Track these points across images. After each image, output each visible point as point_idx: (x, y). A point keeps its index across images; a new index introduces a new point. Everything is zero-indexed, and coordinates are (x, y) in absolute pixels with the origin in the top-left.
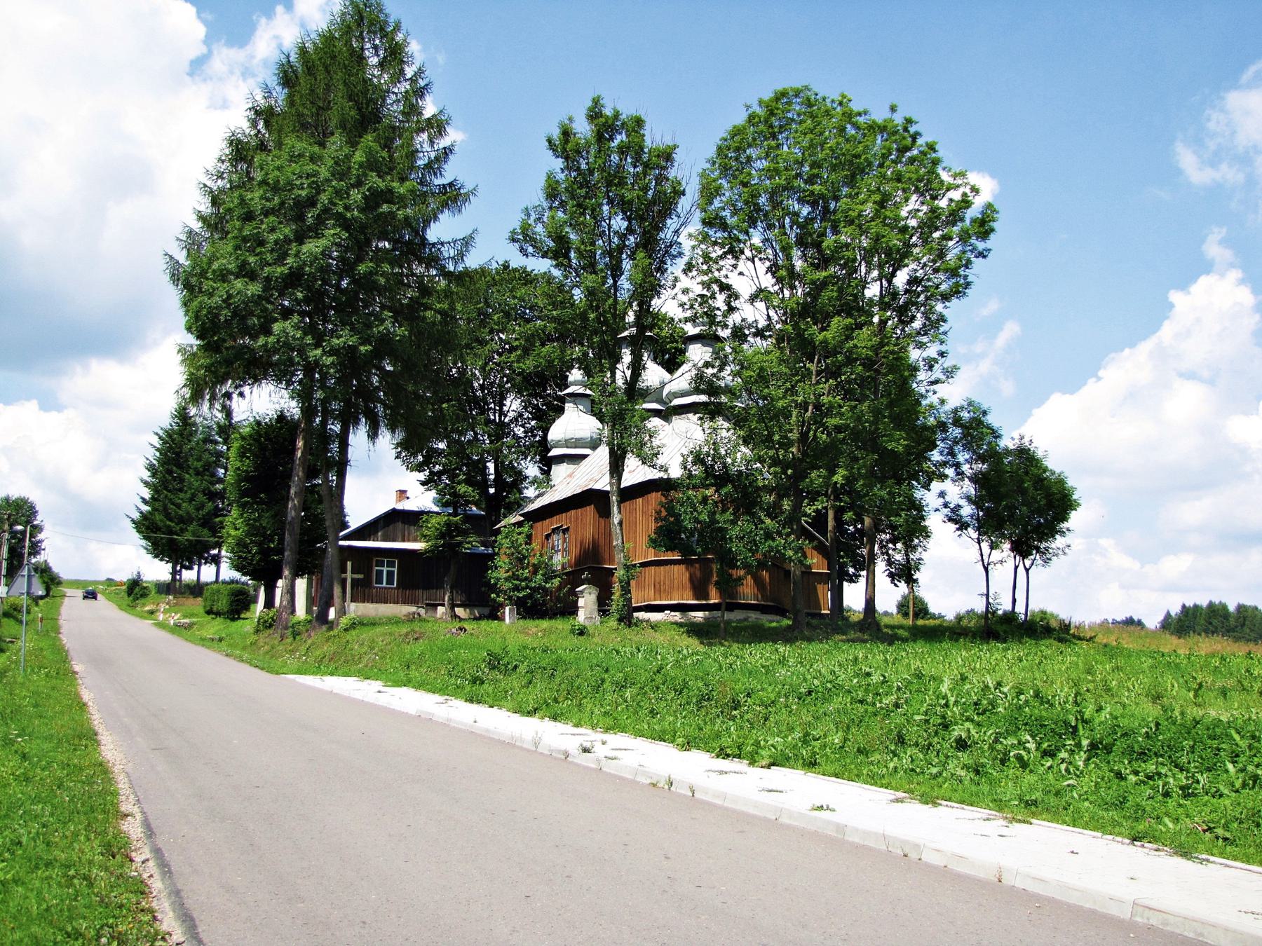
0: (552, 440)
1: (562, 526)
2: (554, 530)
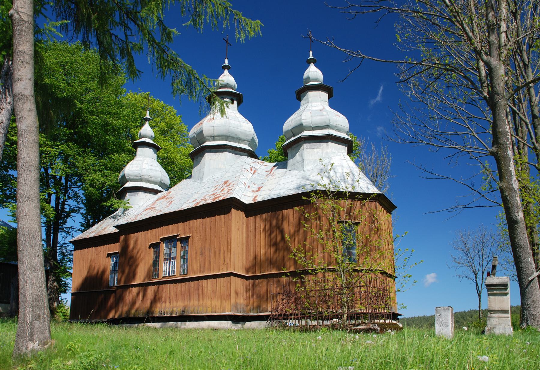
0: (129, 175)
1: (178, 235)
2: (163, 240)
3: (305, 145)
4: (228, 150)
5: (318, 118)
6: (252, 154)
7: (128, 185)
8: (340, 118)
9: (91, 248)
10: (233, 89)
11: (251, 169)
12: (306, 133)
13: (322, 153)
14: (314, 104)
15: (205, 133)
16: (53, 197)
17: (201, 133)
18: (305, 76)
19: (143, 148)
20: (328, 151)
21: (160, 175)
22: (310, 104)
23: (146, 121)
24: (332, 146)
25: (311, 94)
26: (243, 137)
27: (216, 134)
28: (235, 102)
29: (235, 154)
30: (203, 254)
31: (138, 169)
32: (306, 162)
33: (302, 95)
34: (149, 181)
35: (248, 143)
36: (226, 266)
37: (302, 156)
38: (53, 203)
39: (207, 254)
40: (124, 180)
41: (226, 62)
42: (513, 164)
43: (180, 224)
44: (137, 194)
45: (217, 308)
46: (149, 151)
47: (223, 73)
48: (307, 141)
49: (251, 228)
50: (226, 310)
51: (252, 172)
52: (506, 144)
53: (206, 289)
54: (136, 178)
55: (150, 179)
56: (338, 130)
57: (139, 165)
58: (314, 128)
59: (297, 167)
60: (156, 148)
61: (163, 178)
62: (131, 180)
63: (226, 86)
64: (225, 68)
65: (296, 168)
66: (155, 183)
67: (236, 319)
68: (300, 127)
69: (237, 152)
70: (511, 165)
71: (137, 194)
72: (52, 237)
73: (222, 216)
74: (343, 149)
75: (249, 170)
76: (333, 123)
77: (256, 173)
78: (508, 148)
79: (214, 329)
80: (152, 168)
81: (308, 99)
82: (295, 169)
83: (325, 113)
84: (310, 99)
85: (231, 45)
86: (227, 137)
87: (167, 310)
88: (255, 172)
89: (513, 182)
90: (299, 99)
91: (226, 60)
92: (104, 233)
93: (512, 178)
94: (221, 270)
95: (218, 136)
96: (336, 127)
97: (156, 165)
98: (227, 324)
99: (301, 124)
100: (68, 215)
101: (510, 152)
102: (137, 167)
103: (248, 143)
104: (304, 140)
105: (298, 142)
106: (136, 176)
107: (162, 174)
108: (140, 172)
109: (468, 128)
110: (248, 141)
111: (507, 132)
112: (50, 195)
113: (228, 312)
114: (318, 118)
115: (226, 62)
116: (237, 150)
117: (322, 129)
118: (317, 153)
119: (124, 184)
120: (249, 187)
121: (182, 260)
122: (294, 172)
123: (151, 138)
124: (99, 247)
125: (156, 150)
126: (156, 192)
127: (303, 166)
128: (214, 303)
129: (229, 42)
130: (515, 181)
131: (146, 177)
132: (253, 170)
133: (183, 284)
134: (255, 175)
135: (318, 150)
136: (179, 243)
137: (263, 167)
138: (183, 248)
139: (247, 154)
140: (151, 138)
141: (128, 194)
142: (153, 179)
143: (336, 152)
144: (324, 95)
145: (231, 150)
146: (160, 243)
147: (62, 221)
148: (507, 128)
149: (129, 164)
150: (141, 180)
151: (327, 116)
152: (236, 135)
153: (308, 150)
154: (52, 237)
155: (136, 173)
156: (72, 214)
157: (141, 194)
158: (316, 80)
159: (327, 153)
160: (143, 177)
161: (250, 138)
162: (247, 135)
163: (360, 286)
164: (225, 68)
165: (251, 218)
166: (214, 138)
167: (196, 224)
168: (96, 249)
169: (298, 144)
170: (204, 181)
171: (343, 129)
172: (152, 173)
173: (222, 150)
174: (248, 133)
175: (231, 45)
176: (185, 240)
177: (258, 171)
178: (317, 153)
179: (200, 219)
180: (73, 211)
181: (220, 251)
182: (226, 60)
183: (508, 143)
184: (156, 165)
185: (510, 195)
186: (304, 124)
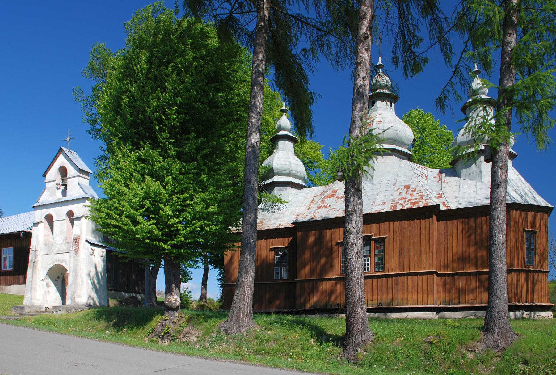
0: (277, 169)
4: (395, 153)
19: (285, 141)
29: (399, 158)
30: (401, 252)
31: (287, 163)
35: (407, 147)
36: (427, 266)
39: (406, 253)
40: (271, 172)
43: (373, 225)
44: (286, 189)
45: (419, 301)
46: (289, 145)
49: (442, 232)
50: (429, 303)
53: (406, 285)
54: (284, 172)
55: (297, 174)
57: (286, 160)
59: (473, 177)
62: (279, 174)
65: (472, 178)
66: (299, 178)
67: (438, 310)
71: (286, 189)
73: (423, 221)
79: (406, 320)
82: (470, 179)
87: (384, 301)
94: (442, 270)
98: (433, 315)
102: (285, 161)
103: (407, 147)
106: (285, 171)
108: (289, 167)
110: (408, 145)
113: (431, 304)
116: (401, 154)
126: (300, 187)
128: (415, 297)
133: (379, 280)
139: (407, 158)
141: (276, 188)
152: (402, 139)
155: (285, 167)
157: (290, 189)
160: (291, 172)
165: (442, 223)
167: (394, 225)
170: (374, 182)
176: (382, 240)
179: (398, 221)
181: (420, 252)
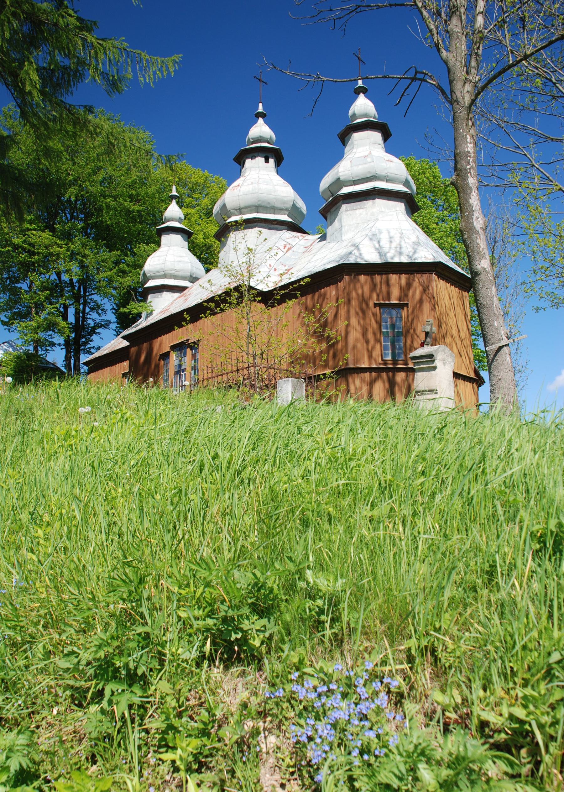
0: (150, 271)
2: (173, 348)
3: (344, 207)
4: (259, 224)
5: (360, 167)
6: (293, 227)
7: (151, 283)
8: (392, 165)
9: (105, 369)
10: (269, 143)
11: (285, 247)
12: (345, 190)
13: (367, 214)
14: (360, 149)
15: (228, 206)
16: (71, 311)
17: (224, 206)
18: (350, 113)
20: (375, 210)
21: (190, 267)
22: (354, 150)
23: (172, 199)
24: (380, 203)
25: (356, 136)
26: (278, 205)
27: (242, 205)
28: (272, 161)
29: (270, 229)
31: (161, 262)
32: (345, 229)
33: (346, 138)
34: (175, 277)
35: (287, 213)
37: (340, 221)
38: (71, 318)
40: (146, 279)
41: (260, 108)
42: (475, 194)
46: (177, 238)
47: (256, 122)
48: (347, 201)
51: (285, 250)
52: (466, 170)
54: (158, 274)
55: (177, 273)
56: (388, 180)
58: (356, 182)
60: (187, 234)
61: (195, 270)
62: (153, 278)
63: (259, 139)
64: (259, 115)
68: (339, 183)
69: (272, 226)
70: (472, 197)
72: (72, 362)
74: (400, 207)
75: (282, 248)
76: (381, 172)
77: (290, 251)
78: (469, 175)
80: (179, 259)
81: (352, 143)
82: (334, 241)
83: (369, 160)
84: (356, 143)
85: (266, 84)
86: (258, 208)
88: (289, 249)
89: (474, 217)
90: (344, 143)
91: (261, 105)
92: (116, 349)
93: (473, 215)
95: (246, 208)
96: (387, 176)
97: (184, 255)
99: (339, 179)
100: (93, 331)
101: (472, 179)
103: (287, 213)
104: (343, 200)
105: (336, 204)
106: (158, 272)
107: (192, 266)
108: (163, 266)
109: (525, 155)
110: (287, 210)
111: (469, 152)
112: (66, 308)
114: (360, 167)
115: (260, 108)
116: (272, 224)
117: (367, 182)
118: (360, 214)
119: (146, 283)
120: (275, 270)
121: (193, 372)
122: (333, 244)
123: (180, 220)
124: (114, 367)
125: (186, 236)
127: (341, 234)
129: (263, 79)
130: (477, 218)
131: (171, 272)
132: (288, 246)
134: (288, 254)
135: (361, 211)
136: (188, 350)
137: (302, 242)
138: (194, 356)
140: (180, 220)
141: (150, 296)
142: (180, 274)
143: (387, 211)
144: (377, 136)
145: (264, 225)
146: (169, 352)
147: (84, 340)
148: (468, 147)
149: (151, 257)
150: (165, 276)
151: (372, 164)
152: (269, 203)
153: (348, 213)
154: (72, 362)
155: (158, 267)
156: (98, 330)
158: (365, 115)
159: (373, 214)
160: (166, 272)
161: (289, 205)
162: (284, 202)
163: (248, 367)
164: (259, 115)
166: (240, 211)
168: (110, 370)
169: (336, 206)
171: (397, 179)
172: (178, 266)
173: (252, 225)
174: (286, 199)
175: (266, 84)
177: (294, 249)
178: (360, 214)
180: (99, 326)
182: (261, 105)
183: (468, 167)
184: (184, 255)
185: (470, 238)
186: (342, 178)
